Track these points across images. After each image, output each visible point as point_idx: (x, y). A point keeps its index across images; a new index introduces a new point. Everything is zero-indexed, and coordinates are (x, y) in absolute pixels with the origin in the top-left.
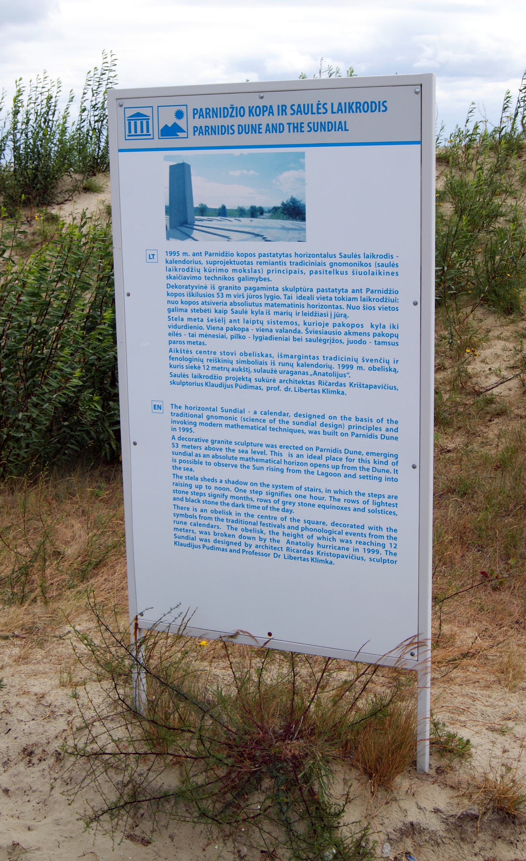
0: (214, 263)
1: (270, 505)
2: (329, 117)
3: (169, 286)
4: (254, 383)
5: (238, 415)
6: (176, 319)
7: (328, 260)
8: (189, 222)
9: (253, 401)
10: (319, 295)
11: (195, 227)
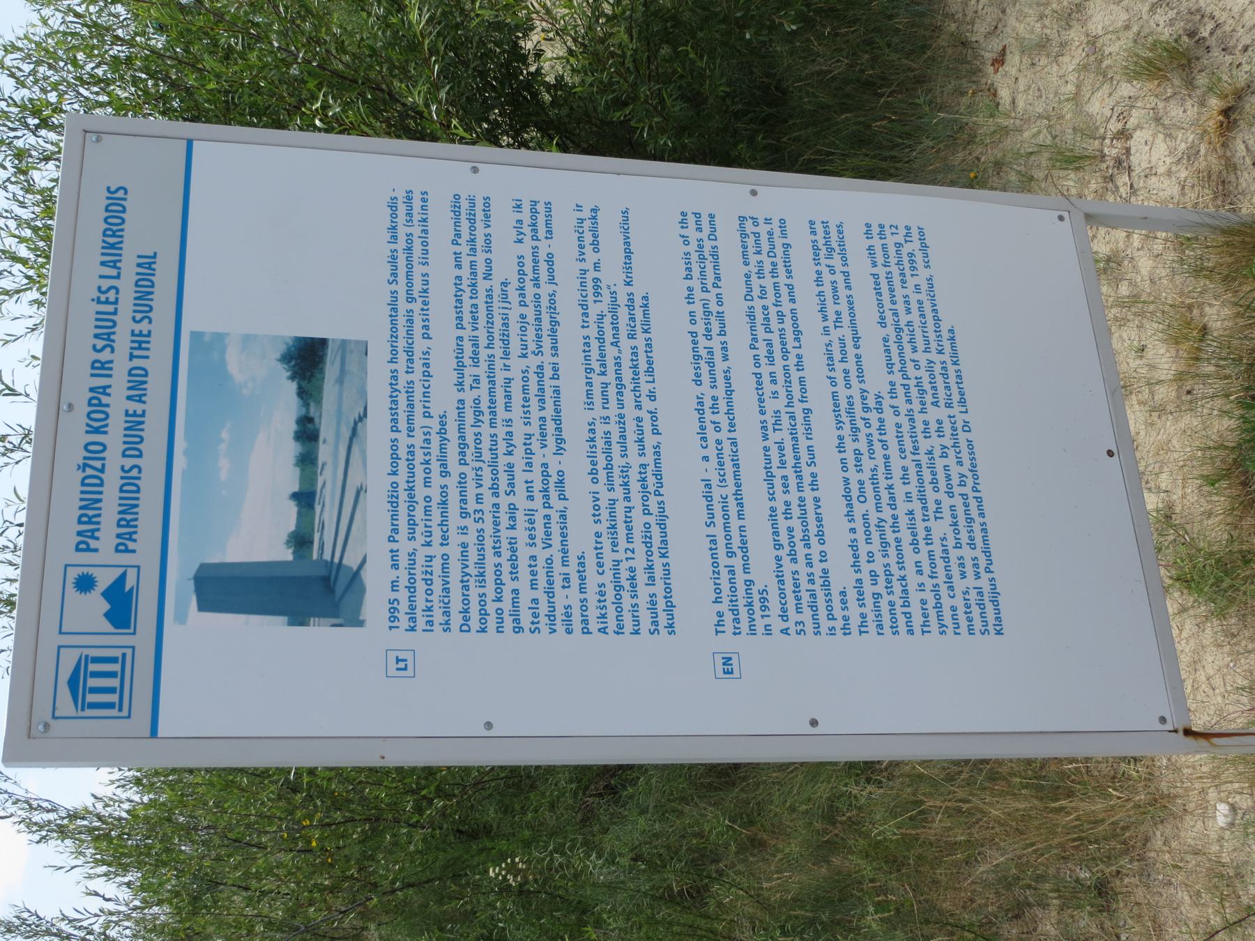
0: (412, 524)
1: (876, 436)
2: (127, 286)
3: (465, 628)
4: (649, 459)
5: (717, 493)
6: (535, 616)
7: (403, 306)
8: (324, 572)
9: (685, 468)
10: (469, 327)
11: (336, 560)
